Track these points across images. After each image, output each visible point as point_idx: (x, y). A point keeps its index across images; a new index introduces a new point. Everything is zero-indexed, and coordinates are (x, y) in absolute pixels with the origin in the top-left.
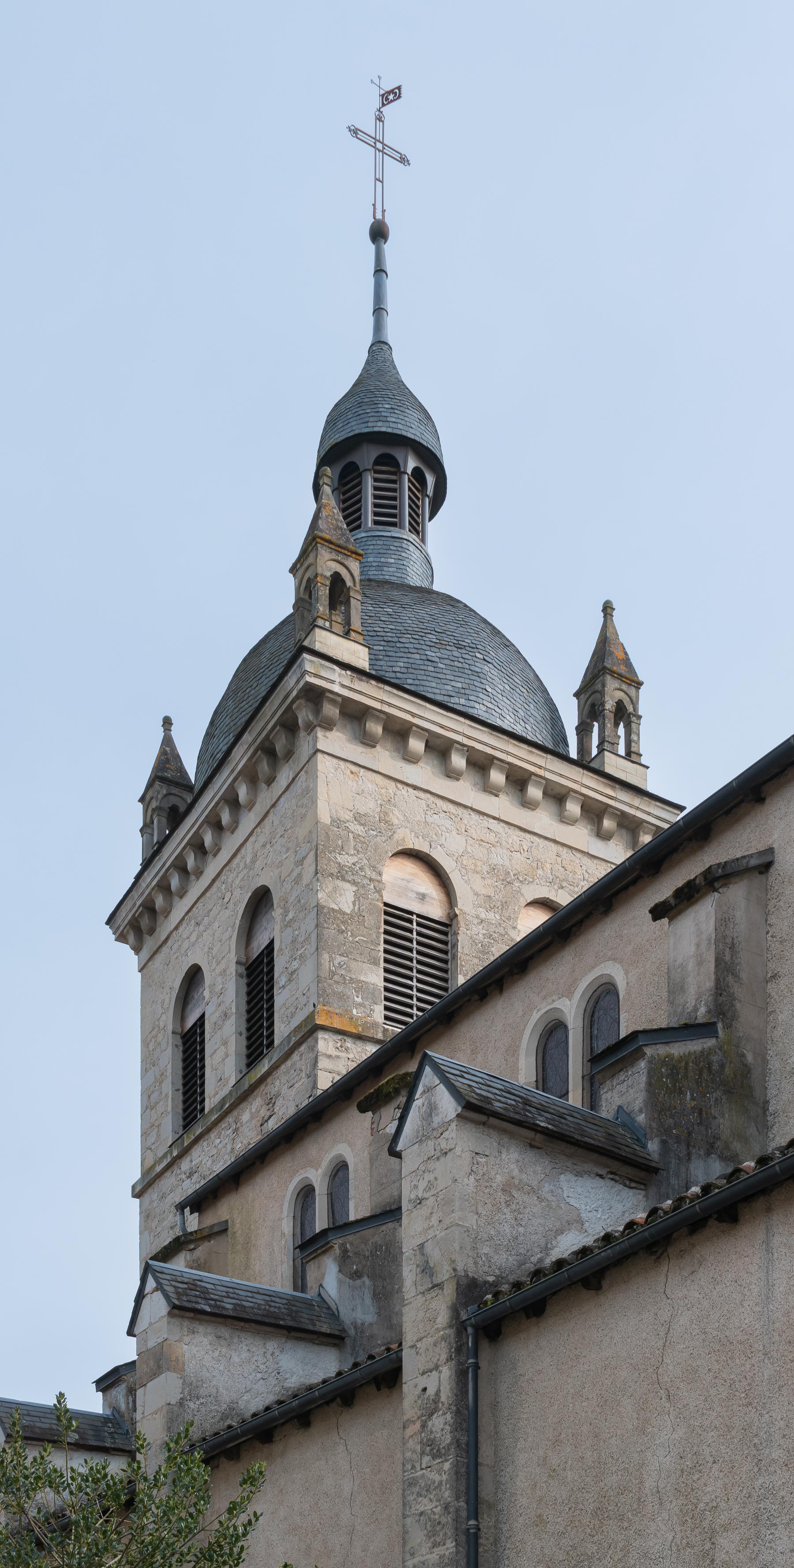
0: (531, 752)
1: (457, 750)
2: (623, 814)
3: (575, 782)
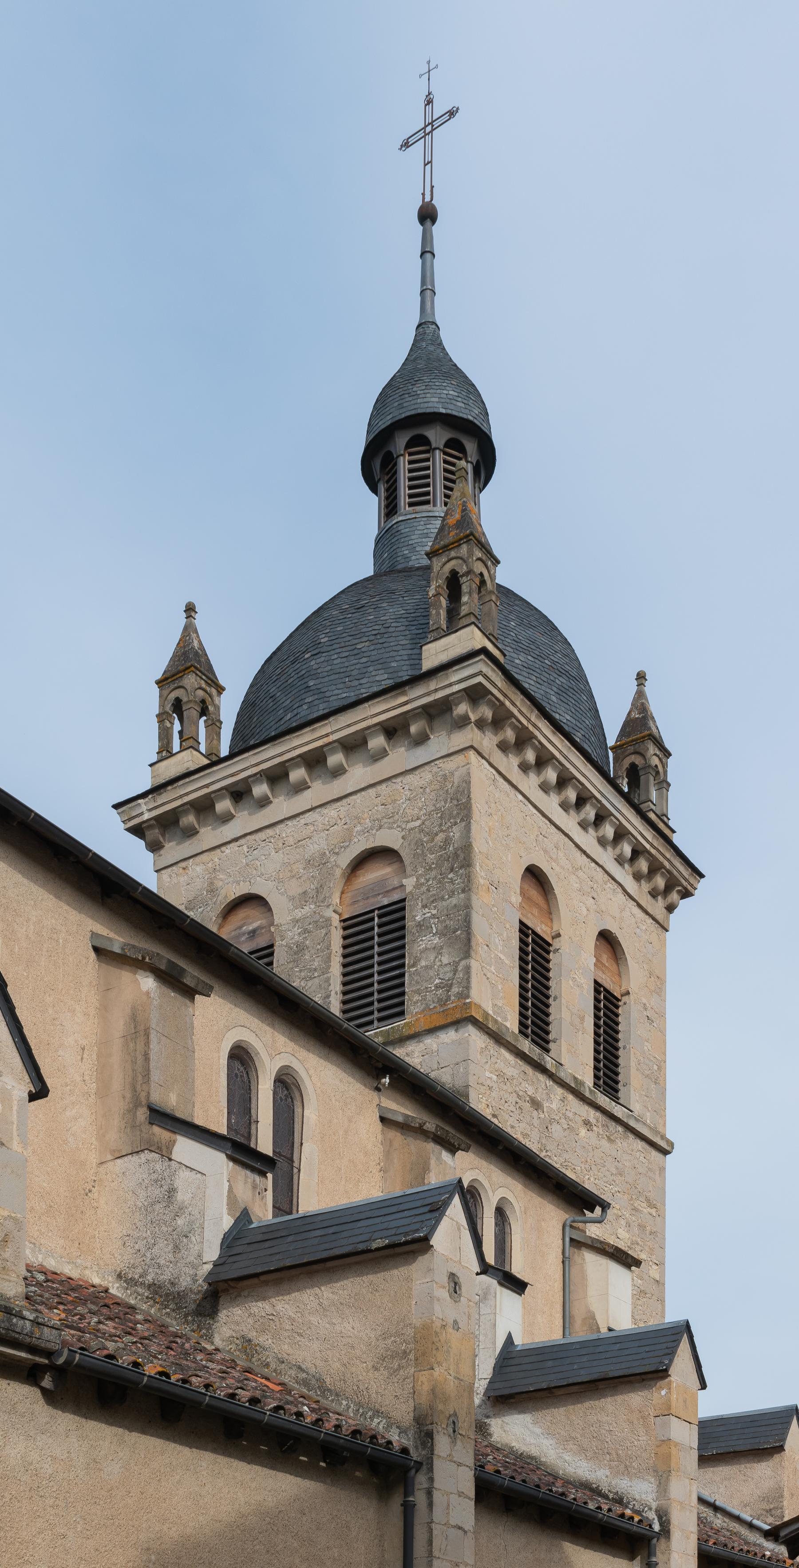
0: (313, 730)
1: (254, 782)
2: (424, 707)
3: (364, 720)
